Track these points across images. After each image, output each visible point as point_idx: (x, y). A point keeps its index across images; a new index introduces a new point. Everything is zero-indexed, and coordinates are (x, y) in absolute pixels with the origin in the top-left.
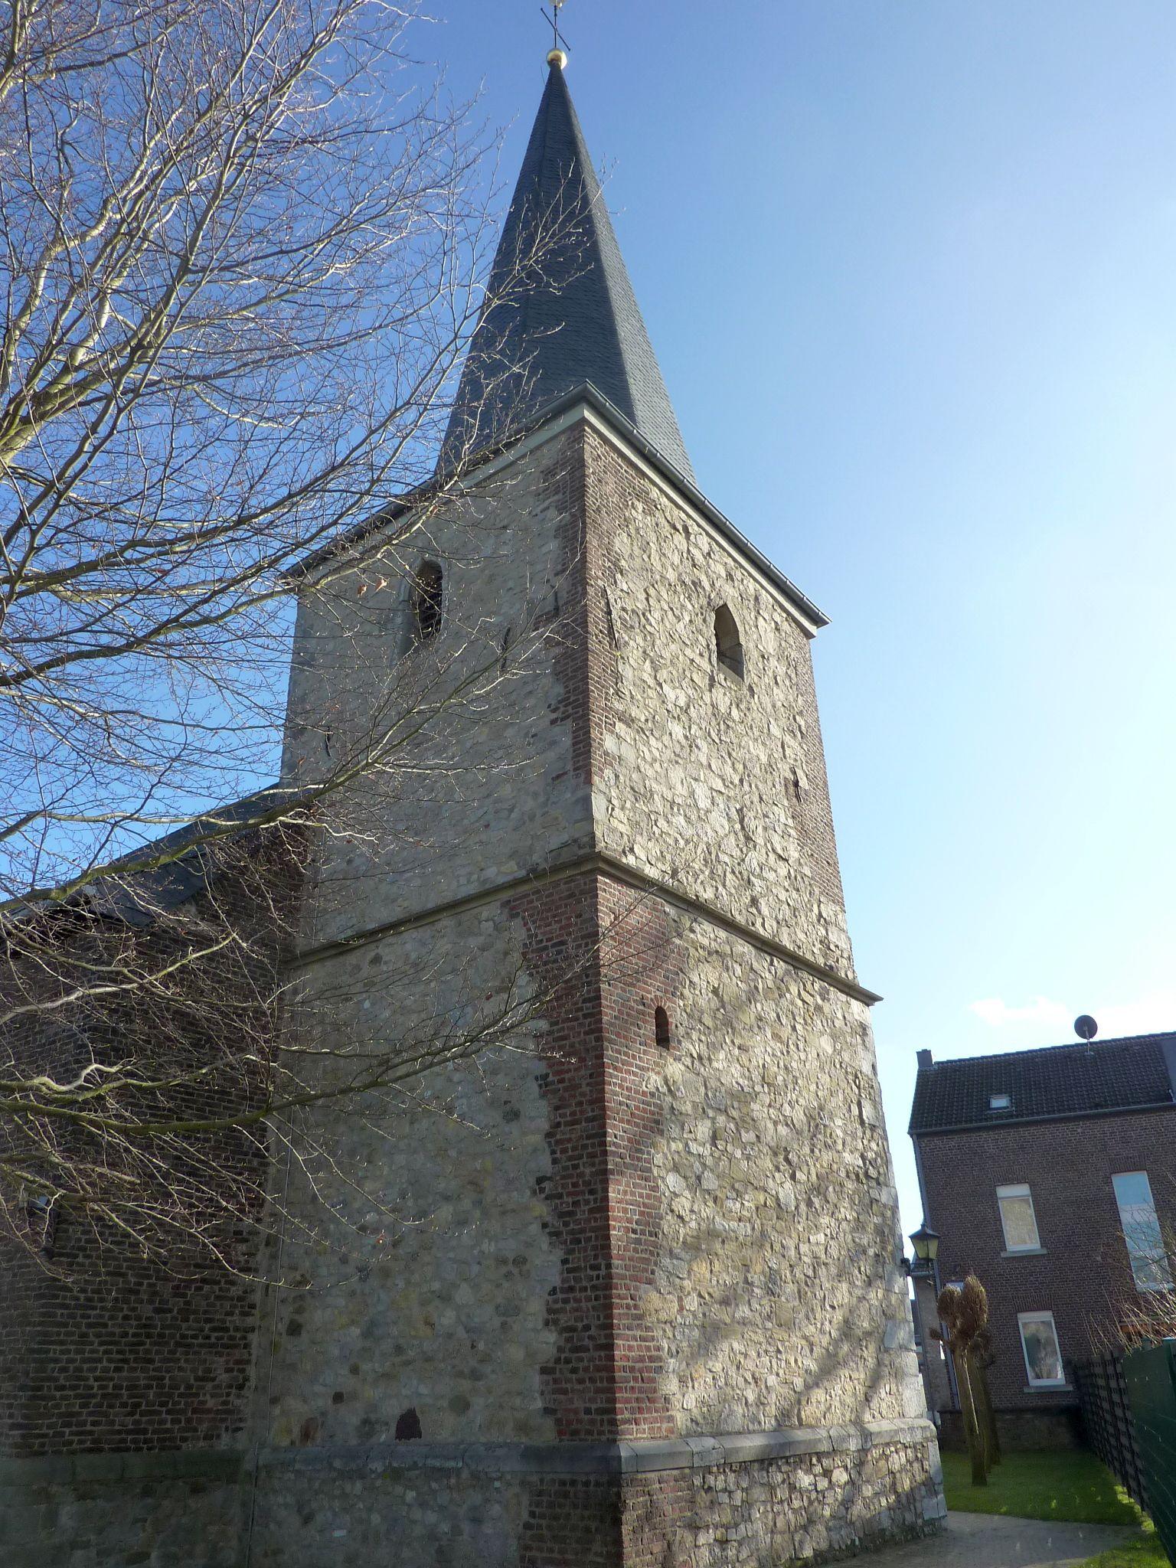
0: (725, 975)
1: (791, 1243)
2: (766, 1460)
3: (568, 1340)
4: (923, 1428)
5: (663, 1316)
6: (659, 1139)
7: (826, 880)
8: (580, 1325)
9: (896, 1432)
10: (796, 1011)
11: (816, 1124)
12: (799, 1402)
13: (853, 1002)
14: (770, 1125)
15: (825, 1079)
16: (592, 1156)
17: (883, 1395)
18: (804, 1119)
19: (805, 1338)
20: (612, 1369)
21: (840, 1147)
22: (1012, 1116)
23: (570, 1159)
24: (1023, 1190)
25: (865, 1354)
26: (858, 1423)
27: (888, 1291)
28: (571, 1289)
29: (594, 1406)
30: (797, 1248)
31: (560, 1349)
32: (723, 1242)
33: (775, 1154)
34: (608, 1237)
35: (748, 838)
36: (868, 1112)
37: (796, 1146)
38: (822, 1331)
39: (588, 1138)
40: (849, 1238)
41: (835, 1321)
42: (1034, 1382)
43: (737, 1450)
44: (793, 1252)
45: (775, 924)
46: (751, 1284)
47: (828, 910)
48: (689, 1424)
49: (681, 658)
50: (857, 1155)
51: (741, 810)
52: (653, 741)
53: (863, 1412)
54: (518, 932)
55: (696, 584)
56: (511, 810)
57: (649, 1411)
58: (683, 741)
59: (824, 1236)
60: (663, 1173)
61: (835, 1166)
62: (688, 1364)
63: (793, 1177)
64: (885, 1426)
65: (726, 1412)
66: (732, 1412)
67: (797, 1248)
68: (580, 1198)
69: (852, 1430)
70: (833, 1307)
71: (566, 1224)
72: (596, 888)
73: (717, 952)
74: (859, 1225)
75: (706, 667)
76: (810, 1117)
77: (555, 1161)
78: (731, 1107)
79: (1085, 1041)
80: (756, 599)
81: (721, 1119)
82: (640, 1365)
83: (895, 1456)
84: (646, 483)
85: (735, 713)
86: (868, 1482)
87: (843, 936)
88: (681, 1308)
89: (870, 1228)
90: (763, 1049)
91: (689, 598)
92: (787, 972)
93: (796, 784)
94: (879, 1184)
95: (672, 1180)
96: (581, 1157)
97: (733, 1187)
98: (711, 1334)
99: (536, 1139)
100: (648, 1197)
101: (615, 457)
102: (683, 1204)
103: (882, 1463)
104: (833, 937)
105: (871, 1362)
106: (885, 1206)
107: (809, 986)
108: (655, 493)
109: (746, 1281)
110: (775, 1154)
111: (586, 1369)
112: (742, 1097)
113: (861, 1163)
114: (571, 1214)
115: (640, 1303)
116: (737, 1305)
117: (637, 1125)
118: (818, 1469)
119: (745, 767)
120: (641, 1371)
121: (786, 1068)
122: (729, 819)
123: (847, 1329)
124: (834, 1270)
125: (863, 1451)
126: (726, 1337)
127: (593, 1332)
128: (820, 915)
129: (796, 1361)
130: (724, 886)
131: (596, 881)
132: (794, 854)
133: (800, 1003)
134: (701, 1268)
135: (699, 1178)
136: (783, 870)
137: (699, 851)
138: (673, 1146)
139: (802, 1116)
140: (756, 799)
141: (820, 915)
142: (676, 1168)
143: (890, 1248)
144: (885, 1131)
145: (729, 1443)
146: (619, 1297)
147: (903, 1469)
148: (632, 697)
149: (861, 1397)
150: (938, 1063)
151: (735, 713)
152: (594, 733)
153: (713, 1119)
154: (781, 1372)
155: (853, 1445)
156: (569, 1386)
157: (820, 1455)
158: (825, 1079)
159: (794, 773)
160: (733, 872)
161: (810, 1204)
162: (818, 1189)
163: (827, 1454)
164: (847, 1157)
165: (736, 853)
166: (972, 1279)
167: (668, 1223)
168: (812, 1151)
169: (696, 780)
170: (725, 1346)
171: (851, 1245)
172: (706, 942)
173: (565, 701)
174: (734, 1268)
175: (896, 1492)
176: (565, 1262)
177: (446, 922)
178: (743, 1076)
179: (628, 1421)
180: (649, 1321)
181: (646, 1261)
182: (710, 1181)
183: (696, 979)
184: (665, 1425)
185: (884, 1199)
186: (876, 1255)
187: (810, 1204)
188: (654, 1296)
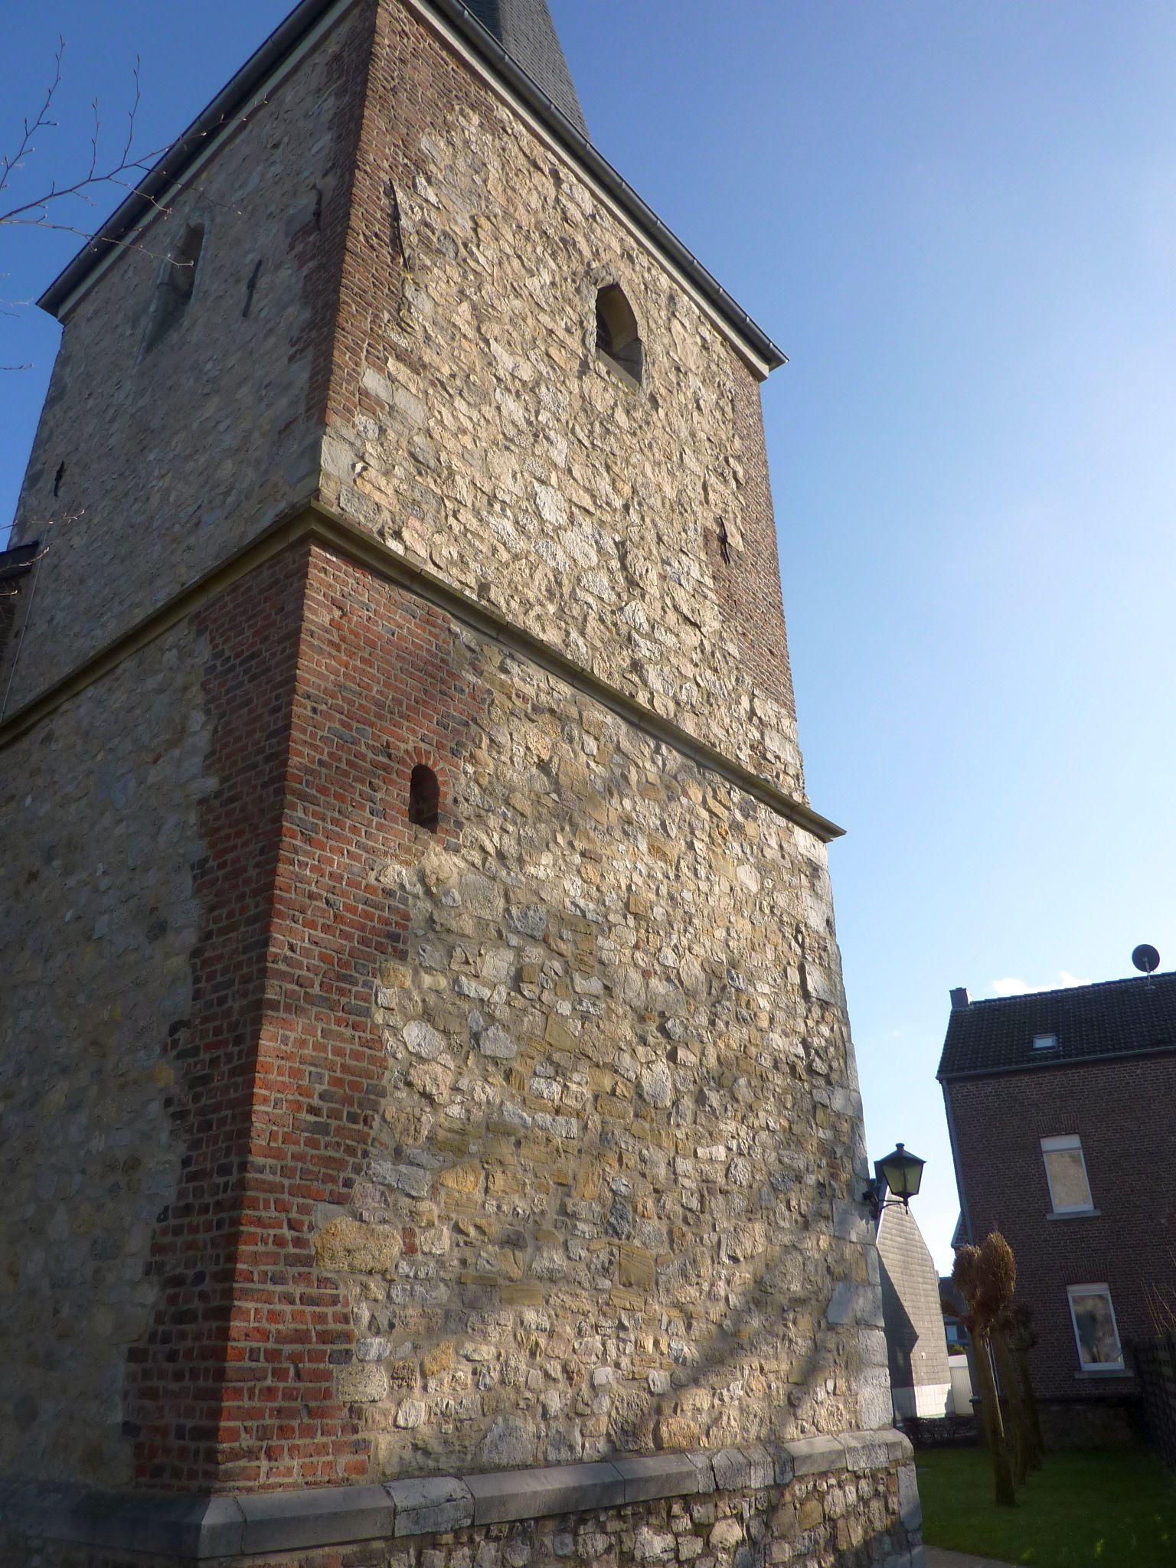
0: (566, 746)
1: (660, 1158)
2: (570, 1514)
3: (172, 1300)
4: (890, 1446)
5: (364, 1260)
6: (393, 964)
7: (770, 669)
8: (190, 1273)
9: (841, 1454)
10: (695, 823)
11: (722, 984)
12: (659, 1411)
13: (797, 830)
14: (635, 976)
15: (743, 925)
16: (246, 979)
17: (821, 1395)
18: (702, 976)
19: (678, 1306)
20: (220, 1354)
21: (765, 1024)
22: (1058, 1057)
23: (217, 988)
24: (1073, 1142)
25: (792, 1332)
26: (774, 1443)
27: (840, 1238)
28: (187, 1210)
29: (189, 1423)
30: (671, 1164)
31: (159, 1318)
32: (518, 1144)
33: (642, 1019)
34: (247, 1116)
35: (632, 583)
36: (815, 981)
37: (682, 1013)
38: (712, 1296)
39: (245, 951)
40: (772, 1157)
41: (737, 1280)
42: (1088, 1366)
43: (503, 1501)
44: (662, 1171)
45: (671, 706)
46: (574, 1216)
47: (766, 709)
48: (408, 1454)
49: (530, 321)
50: (796, 1040)
51: (623, 543)
52: (459, 403)
53: (783, 1425)
54: (203, 652)
55: (568, 243)
56: (227, 493)
57: (308, 1431)
58: (524, 426)
59: (729, 1147)
60: (396, 1020)
61: (753, 1050)
62: (415, 1347)
63: (672, 1056)
64: (822, 1444)
65: (497, 1430)
66: (510, 1432)
67: (671, 1164)
68: (221, 1052)
69: (757, 1455)
70: (734, 1259)
71: (197, 1098)
72: (307, 564)
73: (552, 711)
74: (792, 1139)
75: (573, 342)
76: (712, 973)
77: (197, 995)
78: (565, 942)
79: (1145, 974)
80: (672, 299)
81: (535, 954)
82: (297, 1347)
83: (838, 1492)
84: (491, 99)
85: (620, 416)
86: (783, 1537)
87: (788, 747)
88: (410, 1250)
89: (811, 1145)
90: (628, 866)
91: (554, 256)
92: (683, 768)
93: (723, 539)
94: (829, 1083)
95: (414, 1034)
96: (230, 984)
97: (549, 1059)
98: (474, 1297)
99: (178, 963)
100: (357, 1056)
101: (436, 46)
102: (438, 1075)
103: (813, 1505)
104: (773, 743)
105: (802, 1346)
106: (838, 1115)
107: (722, 794)
108: (504, 114)
109: (563, 1211)
110: (642, 1019)
111: (188, 1354)
112: (583, 927)
113: (801, 1051)
114: (204, 1080)
115: (313, 1237)
116: (539, 1249)
117: (344, 935)
118: (684, 1523)
119: (634, 491)
120: (295, 1358)
121: (672, 898)
122: (600, 550)
123: (760, 1295)
124: (739, 1203)
125: (778, 1487)
126: (511, 1302)
127: (207, 1285)
128: (752, 712)
129: (656, 1343)
130: (583, 634)
131: (309, 553)
132: (711, 621)
133: (705, 814)
134: (465, 1184)
135: (476, 1037)
136: (691, 638)
137: (538, 575)
138: (427, 980)
139: (697, 969)
140: (650, 536)
141: (752, 712)
142: (427, 1016)
143: (844, 1176)
144: (844, 1012)
145: (486, 1488)
146: (259, 1222)
147: (850, 1512)
148: (428, 337)
149: (782, 1400)
150: (974, 1003)
151: (620, 416)
152: (342, 357)
153: (519, 951)
154: (625, 1362)
155: (757, 1479)
156: (161, 1384)
157: (688, 1501)
158: (743, 925)
159: (722, 525)
160: (602, 620)
161: (701, 1099)
162: (722, 1078)
163: (703, 1497)
164: (777, 1040)
165: (609, 596)
166: (995, 1237)
167: (397, 1103)
168: (712, 1023)
169: (542, 482)
170: (508, 1317)
171: (775, 1167)
172: (530, 691)
173: (311, 325)
174: (539, 1188)
175: (836, 1550)
176: (186, 1162)
177: (127, 665)
178: (586, 895)
179: (251, 1454)
180: (327, 1268)
181: (340, 1164)
182: (498, 1044)
183: (503, 739)
184: (344, 1460)
185: (838, 1102)
186: (821, 1185)
187: (701, 1099)
188: (345, 1225)
